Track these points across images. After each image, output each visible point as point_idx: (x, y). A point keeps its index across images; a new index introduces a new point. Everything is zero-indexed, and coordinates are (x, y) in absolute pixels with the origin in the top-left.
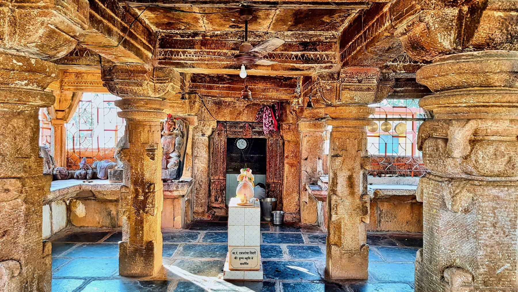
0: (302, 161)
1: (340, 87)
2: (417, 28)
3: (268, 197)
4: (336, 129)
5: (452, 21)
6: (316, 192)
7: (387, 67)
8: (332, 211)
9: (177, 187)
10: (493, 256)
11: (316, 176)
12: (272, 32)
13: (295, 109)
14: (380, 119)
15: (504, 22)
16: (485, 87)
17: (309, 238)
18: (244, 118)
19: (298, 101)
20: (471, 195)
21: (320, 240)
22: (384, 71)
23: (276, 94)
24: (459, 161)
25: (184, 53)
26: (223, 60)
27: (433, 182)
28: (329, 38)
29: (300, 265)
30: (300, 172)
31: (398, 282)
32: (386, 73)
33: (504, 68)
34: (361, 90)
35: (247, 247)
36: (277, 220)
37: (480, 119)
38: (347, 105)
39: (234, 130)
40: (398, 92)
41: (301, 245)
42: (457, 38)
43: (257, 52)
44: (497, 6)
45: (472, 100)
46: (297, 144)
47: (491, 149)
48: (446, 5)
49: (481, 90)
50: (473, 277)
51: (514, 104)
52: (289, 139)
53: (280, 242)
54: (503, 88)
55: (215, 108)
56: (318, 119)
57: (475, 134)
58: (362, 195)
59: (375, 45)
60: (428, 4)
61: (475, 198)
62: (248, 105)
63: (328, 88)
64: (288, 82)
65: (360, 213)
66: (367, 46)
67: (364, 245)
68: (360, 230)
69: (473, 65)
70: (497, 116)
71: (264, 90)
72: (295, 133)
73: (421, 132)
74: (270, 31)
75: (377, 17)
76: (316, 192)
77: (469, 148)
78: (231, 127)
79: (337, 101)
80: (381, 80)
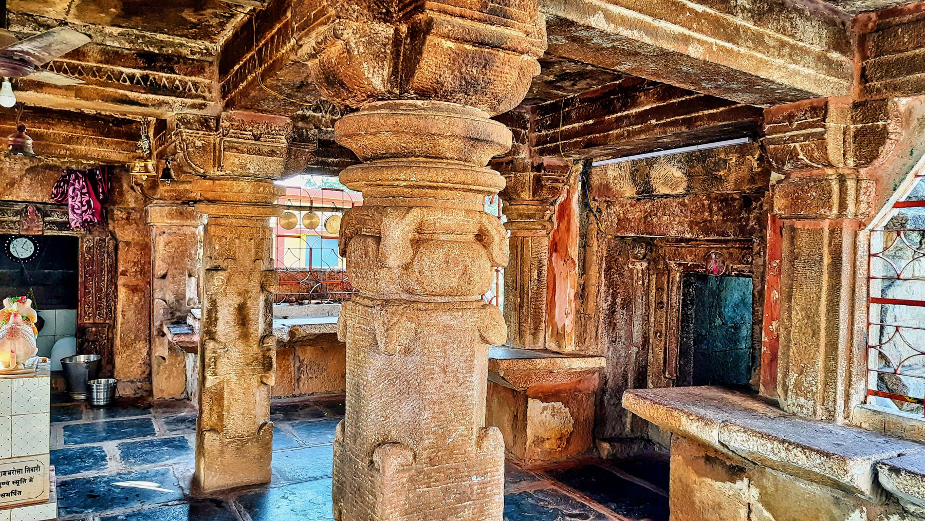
0: (155, 280)
1: (220, 144)
2: (333, 49)
3: (80, 352)
4: (215, 218)
5: (385, 45)
6: (183, 338)
7: (304, 118)
8: (207, 369)
10: (443, 416)
11: (183, 308)
12: (77, 22)
13: (140, 182)
14: (300, 208)
15: (456, 58)
16: (433, 157)
17: (167, 423)
18: (23, 193)
19: (146, 166)
20: (414, 325)
21: (189, 425)
22: (300, 124)
23: (96, 150)
24: (397, 272)
27: (360, 308)
28: (199, 53)
29: (143, 477)
30: (151, 303)
31: (322, 478)
32: (302, 129)
33: (458, 131)
34: (259, 153)
35: (18, 460)
36: (100, 397)
37: (426, 207)
38: (235, 178)
40: (329, 164)
41: (149, 438)
42: (393, 74)
43: (28, 53)
44: (446, 31)
45: (413, 176)
46: (146, 248)
47: (440, 255)
48: (375, 18)
49: (426, 162)
50: (415, 454)
51: (471, 187)
52: (127, 239)
53: (105, 439)
54: (456, 162)
56: (188, 203)
57: (419, 230)
58: (263, 339)
59: (276, 75)
60: (347, 10)
61: (419, 331)
62: (31, 168)
63: (199, 143)
64: (123, 128)
65: (259, 368)
66: (264, 76)
67: (265, 424)
68: (258, 399)
69: (414, 121)
70: (449, 204)
71: (69, 140)
72: (141, 227)
73: (344, 226)
74: (70, 19)
75: (278, 26)
76: (183, 338)
77: (411, 251)
79: (216, 169)
80: (294, 140)
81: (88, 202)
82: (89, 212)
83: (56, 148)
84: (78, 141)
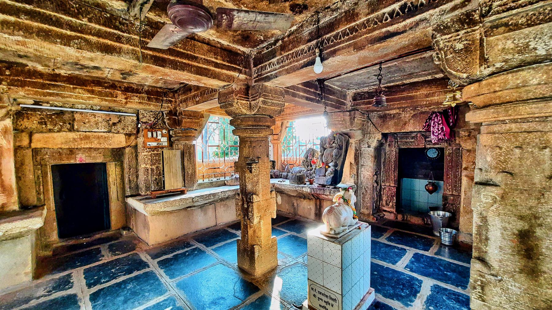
9: (330, 192)
25: (270, 64)
26: (301, 59)
35: (326, 289)
39: (405, 140)
41: (459, 290)
55: (380, 121)
63: (459, 46)
71: (427, 96)
78: (401, 138)
81: (442, 128)
82: (442, 134)
83: (421, 101)
84: (433, 95)
